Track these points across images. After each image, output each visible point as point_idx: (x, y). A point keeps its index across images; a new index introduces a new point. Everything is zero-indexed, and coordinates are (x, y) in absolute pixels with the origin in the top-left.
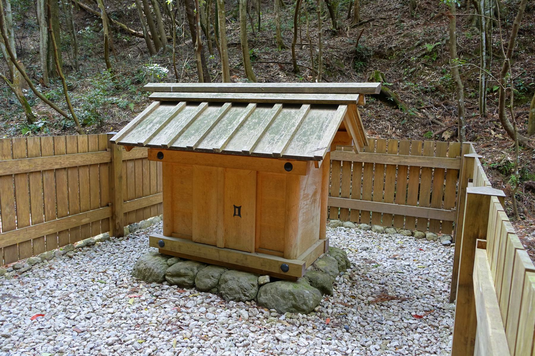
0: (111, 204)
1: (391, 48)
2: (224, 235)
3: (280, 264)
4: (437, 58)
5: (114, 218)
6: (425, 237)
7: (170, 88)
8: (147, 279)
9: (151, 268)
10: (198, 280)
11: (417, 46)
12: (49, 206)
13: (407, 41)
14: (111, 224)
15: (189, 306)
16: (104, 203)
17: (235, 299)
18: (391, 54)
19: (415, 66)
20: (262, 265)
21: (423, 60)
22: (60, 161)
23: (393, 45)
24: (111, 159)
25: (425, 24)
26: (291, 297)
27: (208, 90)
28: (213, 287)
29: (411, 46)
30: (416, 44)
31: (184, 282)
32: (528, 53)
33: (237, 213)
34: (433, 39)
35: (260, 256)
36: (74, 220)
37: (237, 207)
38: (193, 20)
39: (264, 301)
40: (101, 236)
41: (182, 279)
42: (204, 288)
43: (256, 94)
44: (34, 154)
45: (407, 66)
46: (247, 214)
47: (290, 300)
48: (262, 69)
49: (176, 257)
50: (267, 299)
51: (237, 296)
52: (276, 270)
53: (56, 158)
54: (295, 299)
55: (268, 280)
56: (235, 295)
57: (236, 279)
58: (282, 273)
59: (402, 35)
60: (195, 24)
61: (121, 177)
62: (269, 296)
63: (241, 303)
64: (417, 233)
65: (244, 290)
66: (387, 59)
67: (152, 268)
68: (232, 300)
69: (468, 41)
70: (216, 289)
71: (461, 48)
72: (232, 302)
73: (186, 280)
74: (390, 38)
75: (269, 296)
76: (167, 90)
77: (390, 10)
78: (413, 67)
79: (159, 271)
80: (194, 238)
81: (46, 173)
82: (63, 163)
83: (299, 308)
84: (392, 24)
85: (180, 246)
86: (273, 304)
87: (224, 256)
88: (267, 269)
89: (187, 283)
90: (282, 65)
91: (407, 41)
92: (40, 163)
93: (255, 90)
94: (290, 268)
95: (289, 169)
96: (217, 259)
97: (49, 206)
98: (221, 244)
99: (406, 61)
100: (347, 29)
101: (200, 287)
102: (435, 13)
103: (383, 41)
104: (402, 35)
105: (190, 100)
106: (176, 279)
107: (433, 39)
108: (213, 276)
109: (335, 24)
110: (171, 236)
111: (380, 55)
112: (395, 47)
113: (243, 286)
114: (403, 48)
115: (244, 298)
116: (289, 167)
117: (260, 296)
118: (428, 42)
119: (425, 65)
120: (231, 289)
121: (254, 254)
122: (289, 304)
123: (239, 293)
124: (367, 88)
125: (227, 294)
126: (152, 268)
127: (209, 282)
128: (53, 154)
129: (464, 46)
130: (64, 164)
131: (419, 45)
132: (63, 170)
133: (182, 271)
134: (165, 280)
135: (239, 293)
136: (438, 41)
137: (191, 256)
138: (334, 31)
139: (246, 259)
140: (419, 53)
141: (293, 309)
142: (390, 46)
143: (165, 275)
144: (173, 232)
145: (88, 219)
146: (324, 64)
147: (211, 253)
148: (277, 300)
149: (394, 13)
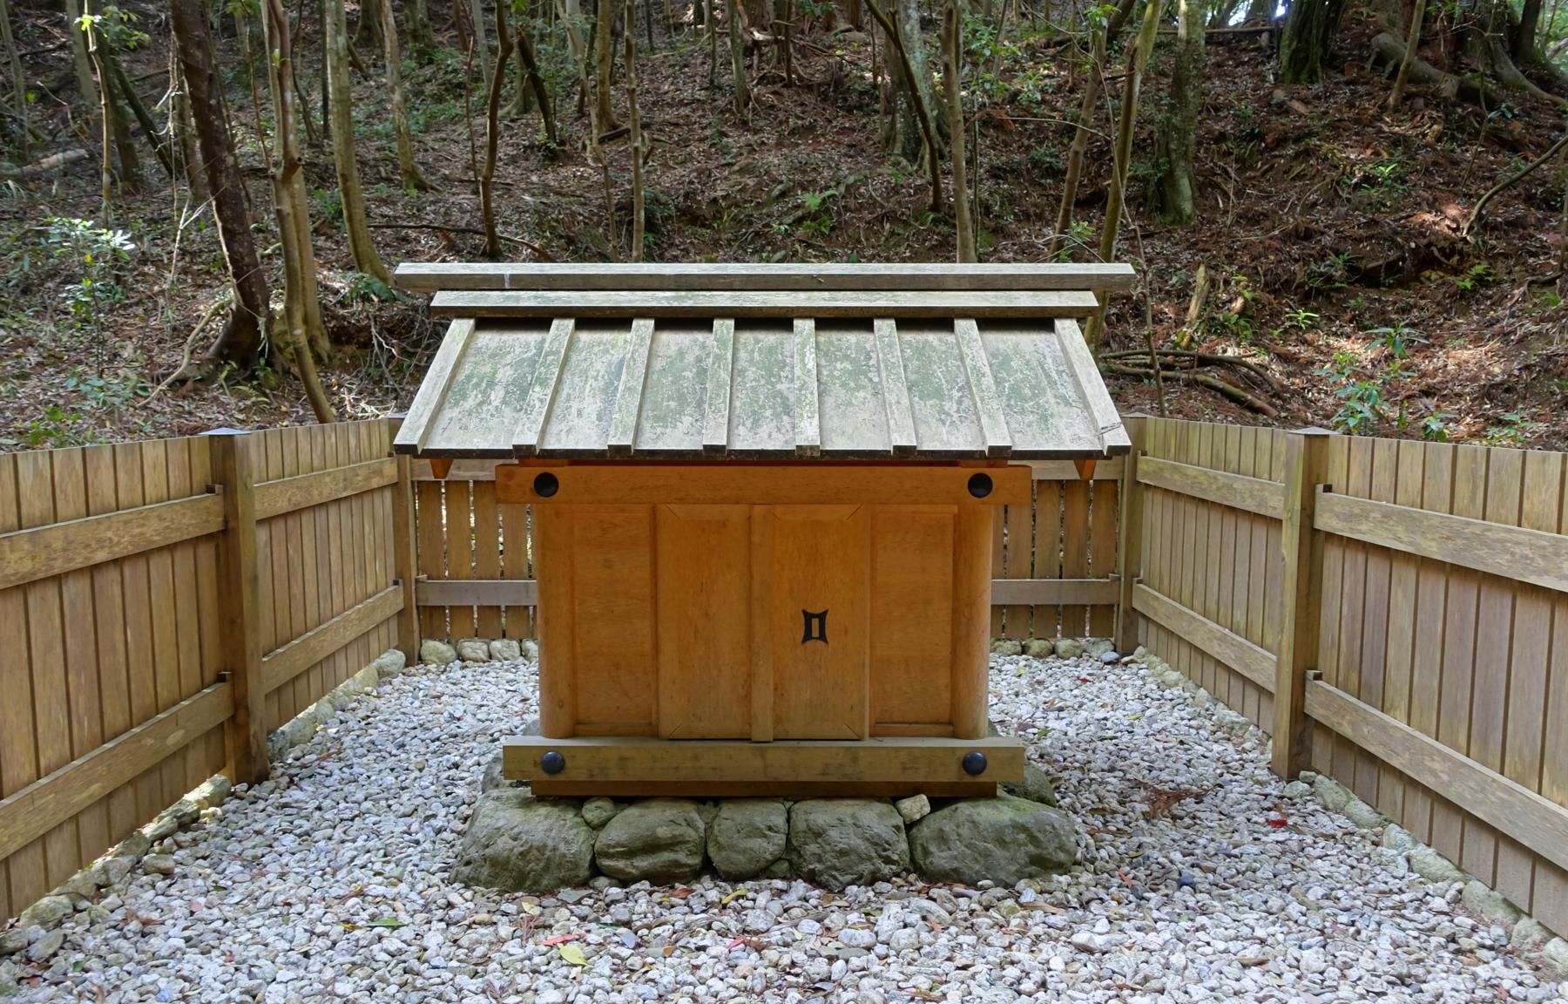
0: (230, 672)
1: (715, 201)
2: (745, 704)
3: (961, 755)
4: (832, 229)
5: (241, 718)
6: (1053, 651)
7: (500, 278)
8: (536, 883)
9: (545, 846)
10: (720, 848)
11: (777, 197)
12: (81, 705)
13: (751, 183)
14: (229, 743)
15: (762, 926)
16: (210, 675)
17: (861, 877)
18: (718, 215)
19: (785, 248)
20: (905, 769)
21: (800, 232)
22: (109, 534)
23: (720, 193)
24: (226, 522)
25: (779, 144)
26: (1022, 836)
27: (640, 284)
28: (777, 860)
29: (765, 197)
30: (776, 192)
31: (677, 864)
32: (1019, 221)
33: (816, 634)
34: (815, 181)
35: (890, 743)
36: (150, 741)
37: (815, 616)
38: (205, 87)
39: (947, 866)
40: (205, 789)
41: (667, 856)
42: (753, 867)
43: (802, 295)
44: (38, 514)
45: (763, 246)
46: (846, 632)
47: (1019, 845)
48: (387, 245)
49: (599, 798)
50: (955, 858)
51: (866, 868)
52: (950, 774)
53: (98, 522)
54: (1033, 840)
55: (927, 809)
56: (860, 868)
57: (849, 821)
58: (968, 779)
59: (736, 168)
60: (210, 98)
61: (255, 579)
62: (959, 848)
63: (882, 886)
64: (1036, 645)
65: (879, 844)
66: (709, 227)
67: (550, 843)
68: (852, 883)
69: (895, 190)
70: (786, 865)
71: (882, 206)
72: (854, 888)
73: (681, 856)
74: (704, 173)
75: (959, 848)
76: (494, 283)
77: (682, 103)
78: (780, 249)
79: (574, 849)
80: (666, 727)
81: (71, 581)
82: (116, 539)
83: (1050, 861)
84: (701, 140)
85: (622, 759)
86: (977, 867)
87: (781, 764)
88: (920, 778)
89: (686, 865)
90: (452, 235)
91: (751, 183)
92: (58, 545)
93: (797, 281)
94: (989, 762)
95: (981, 491)
96: (760, 778)
97: (81, 705)
98: (763, 727)
99: (757, 234)
100: (584, 147)
101: (733, 869)
102: (798, 117)
103: (691, 182)
104: (736, 168)
105: (590, 314)
106: (643, 863)
107: (815, 181)
108: (770, 828)
109: (550, 128)
110: (573, 735)
111: (691, 217)
112: (724, 198)
113: (879, 836)
114: (746, 202)
115: (887, 870)
116: (980, 485)
117: (926, 852)
118: (805, 189)
119: (809, 246)
120: (843, 853)
121: (868, 742)
122: (1022, 857)
123: (870, 859)
124: (1113, 276)
125: (834, 868)
126: (550, 843)
127: (768, 847)
128: (83, 510)
129: (887, 199)
130: (118, 543)
131: (783, 194)
132: (112, 567)
133: (663, 832)
134: (596, 871)
135: (870, 859)
136: (827, 188)
137: (654, 784)
138: (552, 151)
139: (855, 760)
140: (785, 213)
141: (1033, 869)
142: (713, 194)
143: (593, 861)
144: (578, 723)
145: (181, 733)
146: (561, 237)
147: (741, 763)
148: (987, 855)
149: (694, 111)
